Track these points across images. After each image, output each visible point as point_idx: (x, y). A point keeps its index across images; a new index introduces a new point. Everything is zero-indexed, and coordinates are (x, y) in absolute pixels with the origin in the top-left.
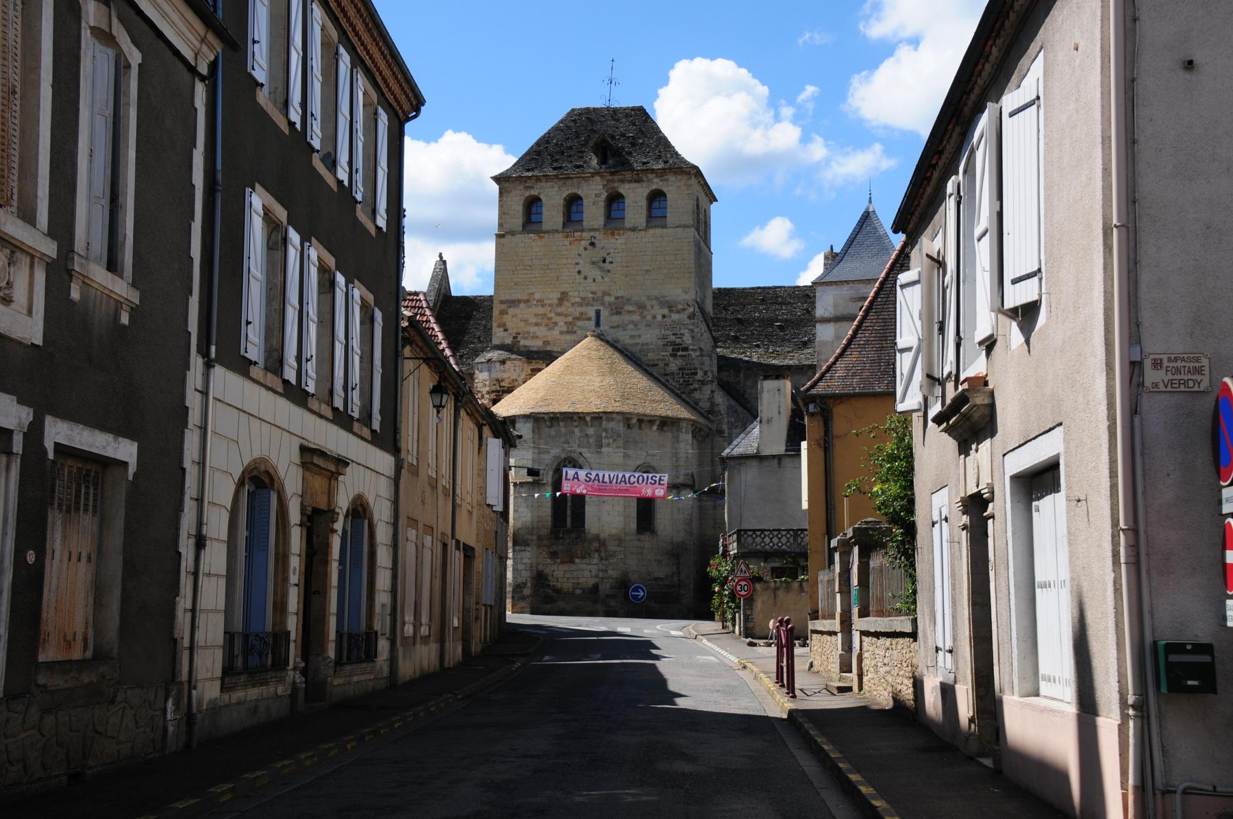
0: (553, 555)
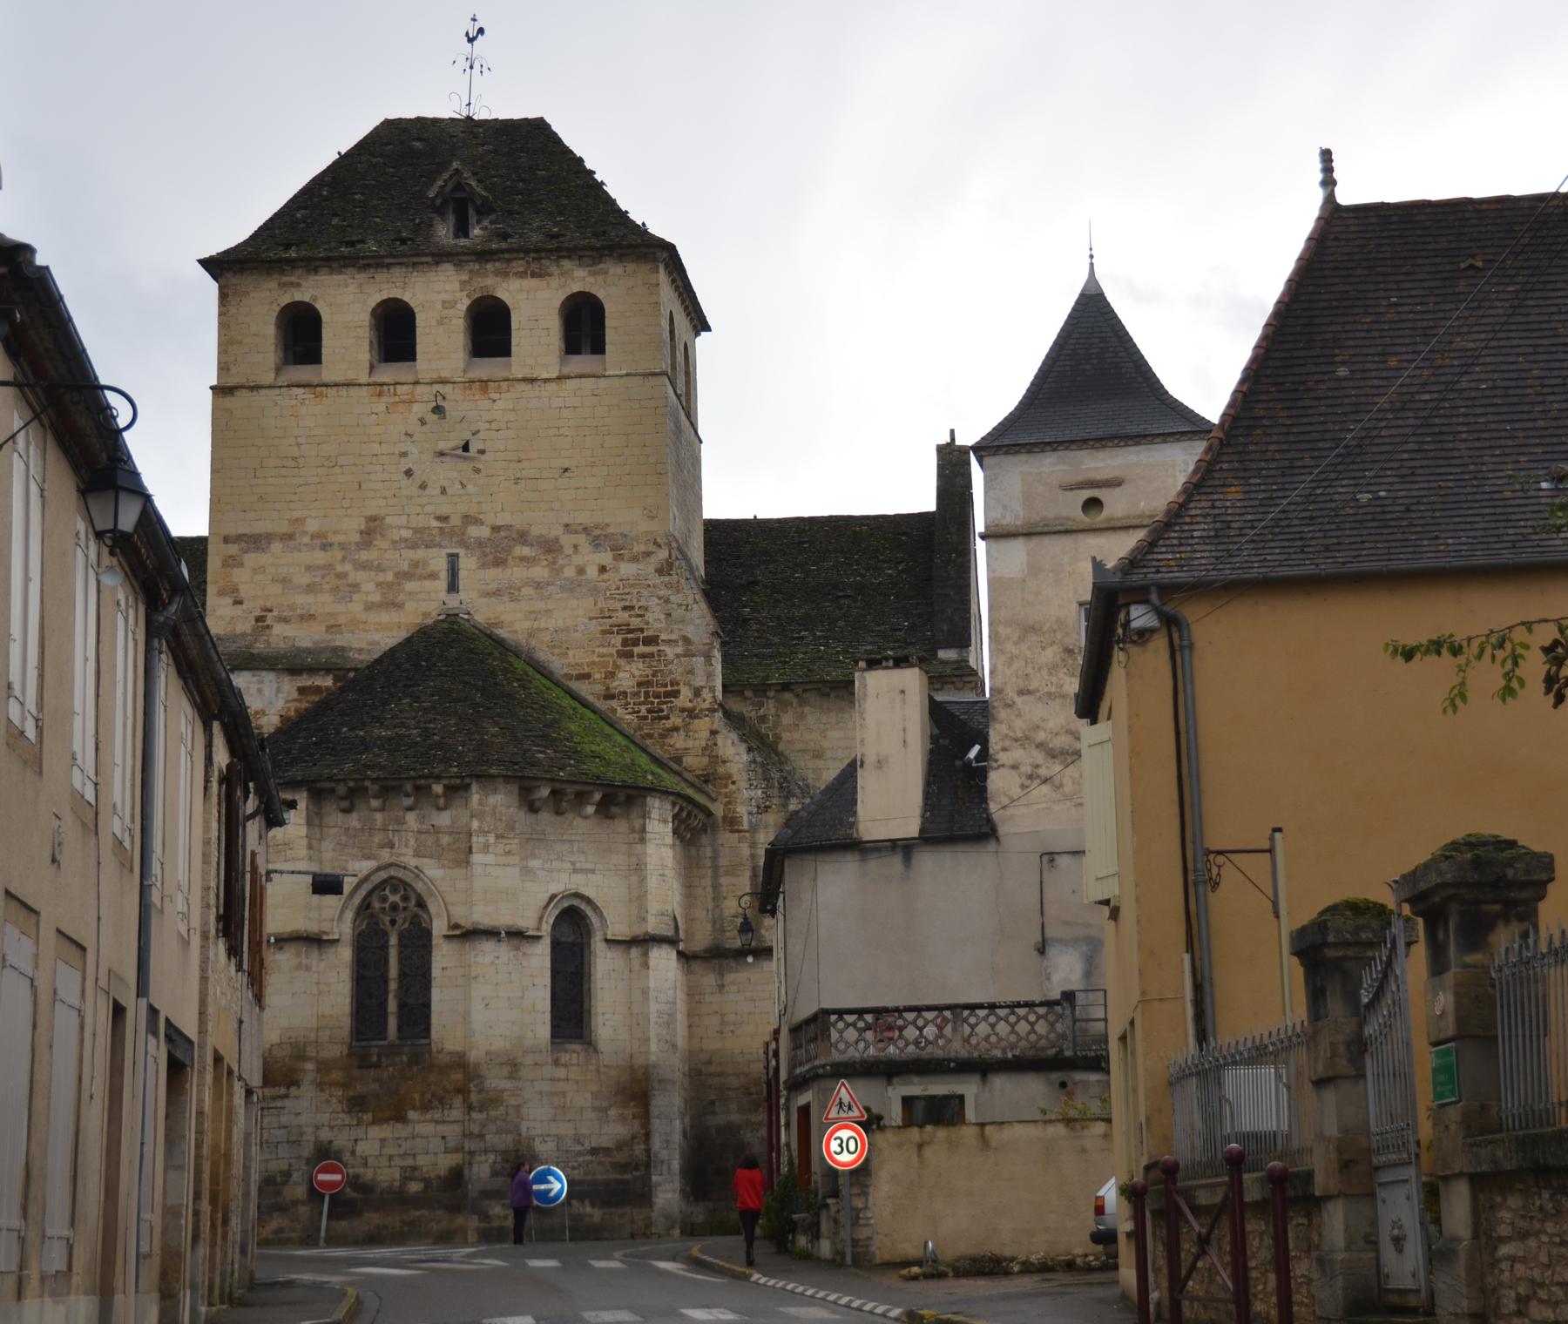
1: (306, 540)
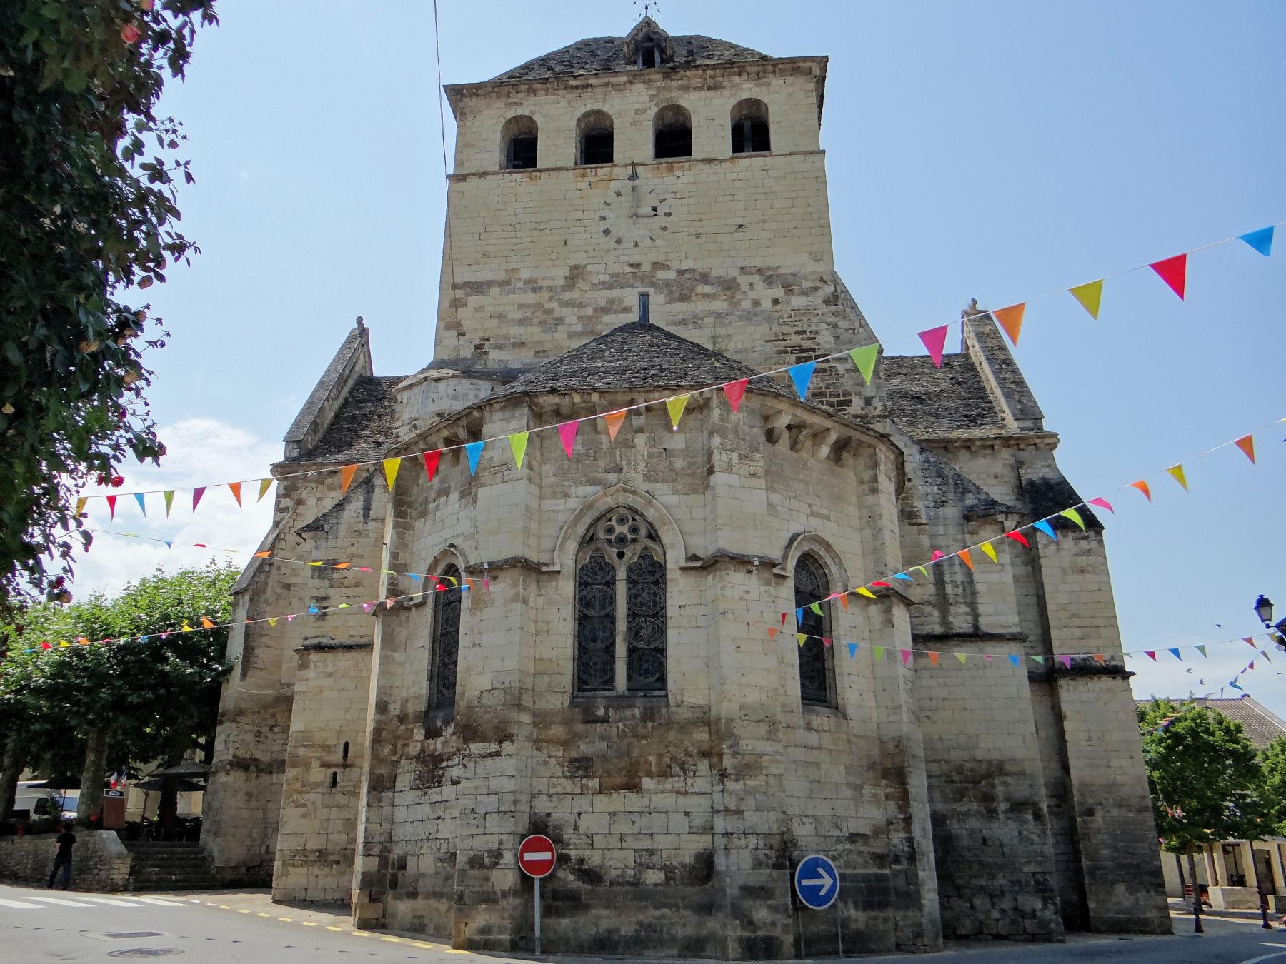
0: (580, 767)
1: (520, 285)
